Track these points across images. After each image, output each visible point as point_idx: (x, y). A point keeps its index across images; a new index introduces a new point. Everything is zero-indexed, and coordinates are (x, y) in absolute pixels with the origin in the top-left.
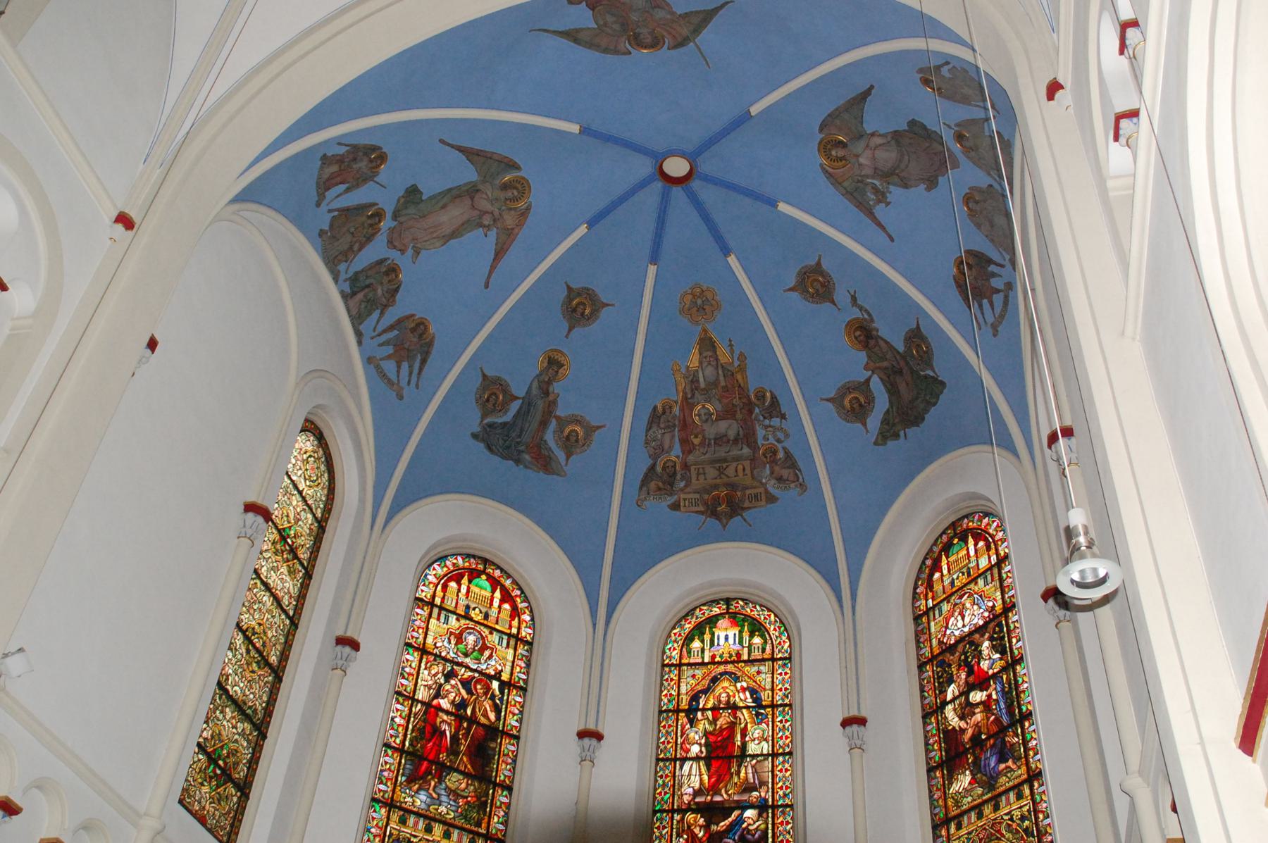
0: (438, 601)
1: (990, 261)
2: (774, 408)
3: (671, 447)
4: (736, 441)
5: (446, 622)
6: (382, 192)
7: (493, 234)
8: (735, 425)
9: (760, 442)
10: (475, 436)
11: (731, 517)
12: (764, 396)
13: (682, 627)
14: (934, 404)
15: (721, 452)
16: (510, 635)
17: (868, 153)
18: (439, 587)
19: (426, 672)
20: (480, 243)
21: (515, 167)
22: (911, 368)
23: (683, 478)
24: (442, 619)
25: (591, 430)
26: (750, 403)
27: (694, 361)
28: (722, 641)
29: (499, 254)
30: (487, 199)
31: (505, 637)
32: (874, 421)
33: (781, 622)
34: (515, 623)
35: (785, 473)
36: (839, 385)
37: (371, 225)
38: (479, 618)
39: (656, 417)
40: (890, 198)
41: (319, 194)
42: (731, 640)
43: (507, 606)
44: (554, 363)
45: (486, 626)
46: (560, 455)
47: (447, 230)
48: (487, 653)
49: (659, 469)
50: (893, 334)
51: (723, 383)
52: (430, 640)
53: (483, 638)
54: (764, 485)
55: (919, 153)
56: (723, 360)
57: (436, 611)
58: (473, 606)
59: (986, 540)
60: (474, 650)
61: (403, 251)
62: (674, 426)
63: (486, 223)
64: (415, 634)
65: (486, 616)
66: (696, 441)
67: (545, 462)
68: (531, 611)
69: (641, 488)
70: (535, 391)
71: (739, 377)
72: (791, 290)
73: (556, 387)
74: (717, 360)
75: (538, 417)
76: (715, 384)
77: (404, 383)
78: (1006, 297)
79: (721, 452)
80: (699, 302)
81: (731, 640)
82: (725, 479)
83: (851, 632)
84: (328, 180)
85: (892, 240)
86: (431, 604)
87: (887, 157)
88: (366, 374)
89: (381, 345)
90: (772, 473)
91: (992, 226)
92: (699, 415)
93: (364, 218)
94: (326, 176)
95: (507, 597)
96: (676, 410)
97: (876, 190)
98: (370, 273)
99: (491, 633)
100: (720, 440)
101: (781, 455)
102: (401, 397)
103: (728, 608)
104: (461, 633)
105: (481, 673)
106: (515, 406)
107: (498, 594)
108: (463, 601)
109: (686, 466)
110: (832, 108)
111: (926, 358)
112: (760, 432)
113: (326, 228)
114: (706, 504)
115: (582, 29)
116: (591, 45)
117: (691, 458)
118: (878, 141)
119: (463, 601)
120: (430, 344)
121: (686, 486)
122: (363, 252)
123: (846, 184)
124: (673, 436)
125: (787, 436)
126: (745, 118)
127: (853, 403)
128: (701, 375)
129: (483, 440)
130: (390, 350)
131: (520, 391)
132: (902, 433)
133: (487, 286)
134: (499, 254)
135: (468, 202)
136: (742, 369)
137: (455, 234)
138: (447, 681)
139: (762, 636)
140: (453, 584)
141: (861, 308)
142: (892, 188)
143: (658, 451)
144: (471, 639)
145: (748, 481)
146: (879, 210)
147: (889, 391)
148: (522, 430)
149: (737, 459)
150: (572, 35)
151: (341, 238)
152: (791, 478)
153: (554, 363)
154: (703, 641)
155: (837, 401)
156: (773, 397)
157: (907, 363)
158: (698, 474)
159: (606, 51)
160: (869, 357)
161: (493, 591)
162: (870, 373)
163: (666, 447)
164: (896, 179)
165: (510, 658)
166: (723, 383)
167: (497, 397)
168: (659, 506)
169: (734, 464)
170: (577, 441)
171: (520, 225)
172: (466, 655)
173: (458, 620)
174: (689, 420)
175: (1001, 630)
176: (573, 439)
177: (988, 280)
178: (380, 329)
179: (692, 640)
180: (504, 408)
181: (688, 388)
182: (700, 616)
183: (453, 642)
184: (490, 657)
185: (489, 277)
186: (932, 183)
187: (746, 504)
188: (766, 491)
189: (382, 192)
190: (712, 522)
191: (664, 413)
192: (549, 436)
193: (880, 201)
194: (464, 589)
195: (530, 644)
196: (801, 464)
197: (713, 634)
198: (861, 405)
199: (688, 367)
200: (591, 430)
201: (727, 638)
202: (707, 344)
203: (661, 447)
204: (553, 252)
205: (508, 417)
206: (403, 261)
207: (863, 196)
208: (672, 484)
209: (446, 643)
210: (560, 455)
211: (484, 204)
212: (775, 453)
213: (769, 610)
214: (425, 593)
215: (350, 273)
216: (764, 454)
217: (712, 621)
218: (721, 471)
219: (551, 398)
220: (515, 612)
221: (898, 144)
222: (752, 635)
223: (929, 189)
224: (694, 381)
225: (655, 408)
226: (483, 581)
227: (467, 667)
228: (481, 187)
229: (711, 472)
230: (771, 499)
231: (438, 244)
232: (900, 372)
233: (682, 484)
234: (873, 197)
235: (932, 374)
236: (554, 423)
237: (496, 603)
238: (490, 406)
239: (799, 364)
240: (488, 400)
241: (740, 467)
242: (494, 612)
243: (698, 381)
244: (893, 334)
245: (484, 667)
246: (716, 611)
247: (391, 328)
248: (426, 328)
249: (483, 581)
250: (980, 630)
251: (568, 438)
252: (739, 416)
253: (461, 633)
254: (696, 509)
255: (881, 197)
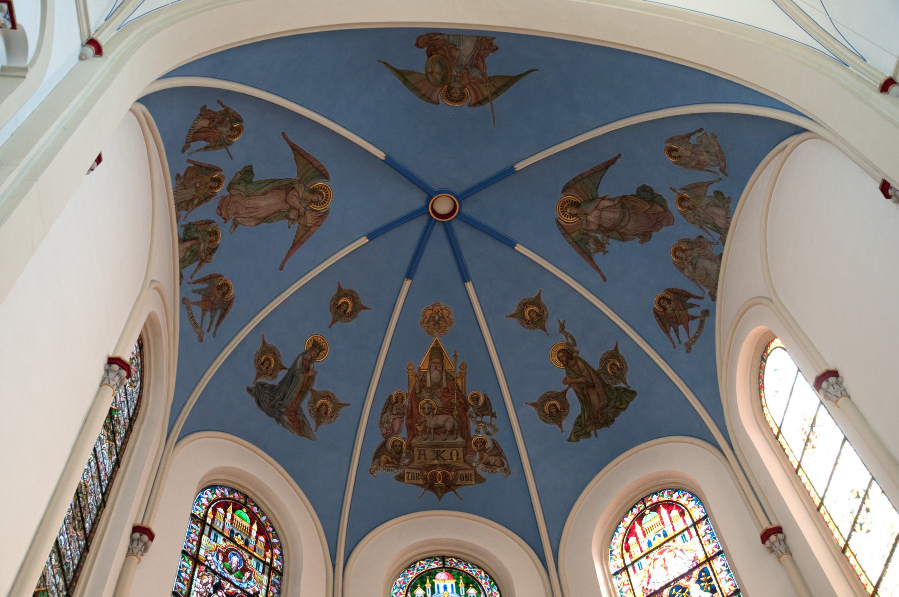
0: (209, 521)
1: (689, 296)
2: (486, 408)
3: (400, 430)
4: (452, 432)
5: (215, 540)
6: (227, 162)
7: (295, 226)
8: (451, 419)
9: (473, 433)
10: (249, 390)
11: (446, 491)
12: (478, 398)
13: (405, 576)
14: (624, 409)
15: (439, 440)
16: (265, 563)
17: (596, 212)
18: (210, 510)
19: (198, 580)
20: (283, 232)
21: (325, 176)
22: (603, 382)
23: (407, 456)
24: (212, 538)
25: (338, 406)
26: (466, 402)
27: (424, 363)
28: (442, 590)
29: (297, 244)
30: (298, 197)
31: (261, 564)
32: (568, 424)
33: (490, 577)
34: (269, 554)
35: (492, 460)
36: (543, 393)
37: (211, 188)
38: (241, 543)
39: (391, 405)
40: (608, 248)
41: (187, 142)
42: (449, 589)
43: (262, 538)
44: (317, 347)
45: (247, 551)
46: (312, 422)
47: (262, 214)
48: (247, 574)
49: (389, 446)
50: (591, 356)
51: (445, 385)
52: (202, 552)
53: (244, 561)
54: (474, 468)
55: (645, 210)
56: (448, 367)
57: (207, 529)
58: (236, 532)
59: (678, 508)
60: (237, 570)
61: (226, 220)
62: (404, 414)
63: (292, 217)
64: (190, 545)
65: (247, 543)
66: (420, 429)
67: (300, 426)
68: (281, 547)
69: (374, 460)
70: (298, 366)
71: (459, 382)
72: (511, 316)
73: (315, 366)
74: (443, 366)
75: (299, 386)
76: (439, 385)
77: (205, 328)
78: (702, 322)
79: (439, 440)
80: (437, 318)
81: (449, 589)
82: (442, 462)
83: (747, 483)
84: (198, 131)
85: (605, 280)
86: (203, 522)
87: (611, 216)
88: (180, 310)
89: (194, 291)
90: (481, 459)
91: (695, 268)
92: (423, 408)
93: (207, 179)
94: (198, 128)
95: (261, 532)
96: (406, 402)
97: (597, 241)
98: (200, 228)
99: (250, 558)
100: (438, 430)
101: (489, 445)
102: (201, 340)
103: (444, 564)
104: (227, 552)
105: (242, 589)
106: (282, 374)
107: (255, 527)
108: (228, 527)
109: (410, 447)
110: (577, 174)
111: (620, 372)
112: (473, 426)
113: (182, 174)
114: (425, 478)
115: (413, 72)
116: (414, 89)
117: (414, 441)
118: (606, 203)
119: (228, 527)
120: (230, 303)
121: (410, 463)
122: (201, 207)
123: (573, 235)
124: (402, 422)
125: (496, 430)
126: (510, 171)
127: (551, 410)
128: (428, 376)
129: (254, 395)
130: (199, 298)
131: (287, 362)
132: (593, 433)
133: (281, 268)
134: (297, 244)
135: (283, 194)
136: (462, 376)
137: (265, 219)
138: (215, 592)
139: (476, 588)
140: (221, 510)
141: (567, 334)
142: (610, 240)
143: (390, 432)
144: (235, 559)
145: (461, 463)
146: (598, 257)
147: (581, 401)
148: (284, 395)
149: (451, 446)
150: (403, 76)
151: (192, 186)
152: (497, 464)
153: (317, 347)
154: (424, 589)
155: (539, 406)
156: (486, 399)
157: (600, 379)
158: (420, 455)
159: (423, 96)
160: (568, 373)
161: (252, 524)
162: (567, 386)
163: (396, 430)
164: (615, 234)
165: (265, 581)
166: (445, 385)
167: (270, 363)
168: (388, 476)
169: (450, 450)
170: (326, 413)
171: (317, 225)
172: (231, 572)
173: (224, 540)
174: (415, 412)
175: (708, 574)
176: (323, 411)
177: (685, 310)
178: (196, 278)
179: (415, 587)
180: (273, 374)
181: (417, 384)
182: (419, 568)
183: (221, 558)
184: (250, 579)
185: (284, 262)
186: (645, 236)
187: (459, 482)
188: (476, 473)
189: (227, 162)
190: (430, 495)
191: (397, 402)
192: (305, 405)
193: (598, 250)
194: (229, 516)
195: (281, 574)
196: (506, 453)
197: (433, 584)
198: (557, 411)
199: (420, 369)
200: (338, 406)
201: (445, 588)
202: (437, 352)
203: (392, 428)
204: (336, 254)
205: (276, 382)
206: (224, 229)
207: (585, 244)
208: (398, 460)
209: (215, 558)
210: (312, 422)
211: (294, 201)
212: (484, 443)
213: (479, 568)
214: (200, 512)
215: (185, 223)
216: (475, 444)
217: (432, 574)
218: (438, 455)
219: (310, 374)
220: (269, 546)
221: (623, 206)
222: (467, 586)
223: (642, 242)
224: (423, 381)
225: (391, 396)
226: (243, 513)
227: (232, 583)
228: (296, 186)
229: (430, 454)
230: (480, 479)
231: (252, 224)
232: (594, 386)
233: (407, 461)
234: (593, 246)
235: (623, 385)
236: (310, 394)
237: (254, 534)
238: (264, 368)
239: (510, 376)
240: (263, 364)
241: (454, 453)
242: (252, 540)
243: (426, 381)
244: (591, 356)
245: (245, 586)
246: (434, 565)
247: (204, 280)
248: (228, 290)
249: (243, 513)
250: (688, 575)
251: (319, 409)
252: (456, 413)
253: (227, 552)
254: (415, 482)
255: (601, 247)
